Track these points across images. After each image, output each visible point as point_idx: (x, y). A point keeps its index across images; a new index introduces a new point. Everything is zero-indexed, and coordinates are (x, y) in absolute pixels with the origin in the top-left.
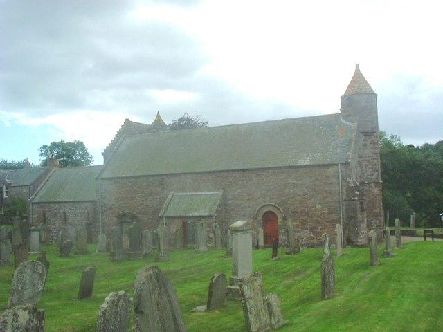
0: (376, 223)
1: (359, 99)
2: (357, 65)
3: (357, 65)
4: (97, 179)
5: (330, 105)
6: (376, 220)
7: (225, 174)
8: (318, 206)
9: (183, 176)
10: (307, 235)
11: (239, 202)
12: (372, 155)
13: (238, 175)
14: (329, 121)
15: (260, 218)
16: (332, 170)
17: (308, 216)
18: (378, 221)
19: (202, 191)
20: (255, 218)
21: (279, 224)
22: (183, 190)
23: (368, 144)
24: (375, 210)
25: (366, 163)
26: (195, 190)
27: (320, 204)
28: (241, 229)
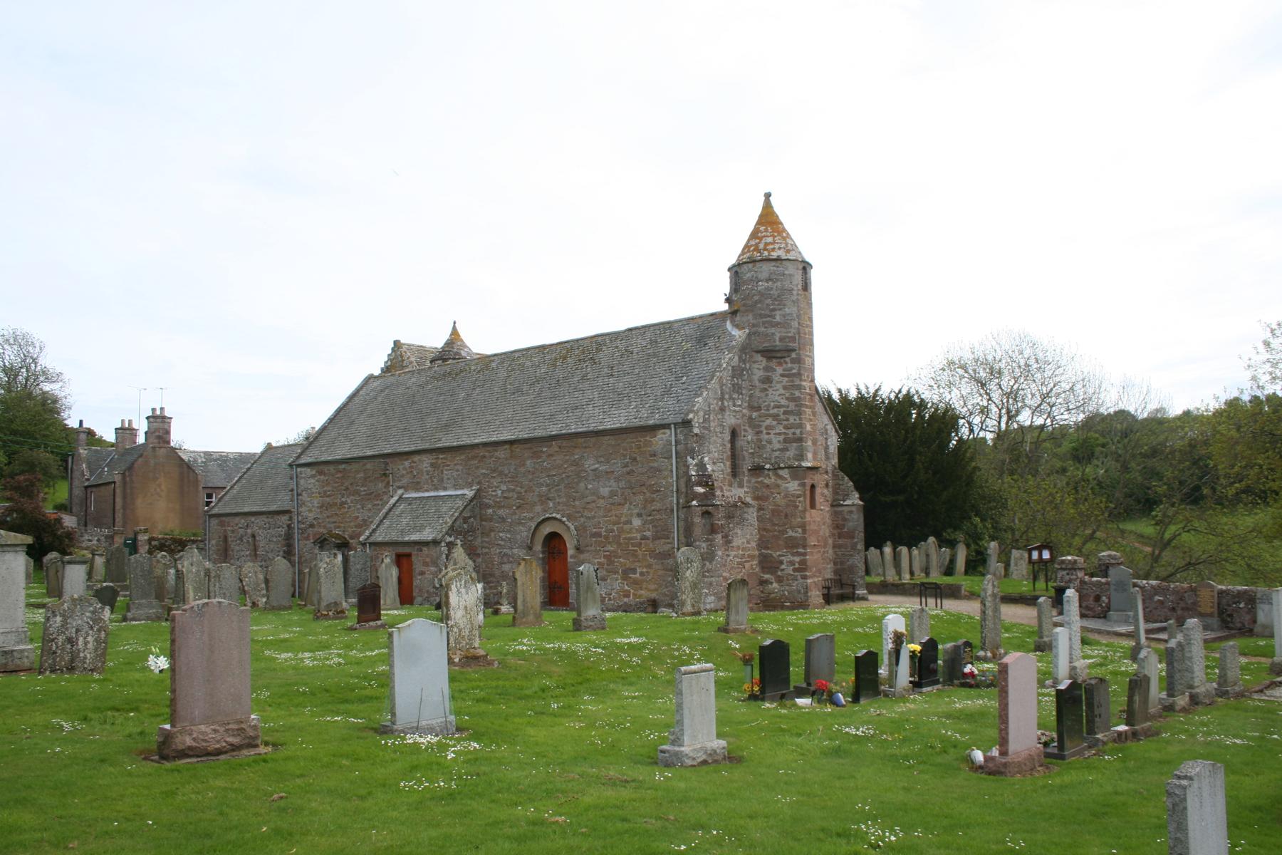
0: (792, 563)
1: (769, 284)
2: (768, 196)
3: (768, 196)
4: (290, 465)
5: (696, 287)
6: (793, 555)
7: (481, 452)
8: (637, 522)
9: (416, 458)
10: (617, 585)
11: (501, 512)
12: (783, 402)
13: (501, 453)
14: (702, 330)
15: (538, 547)
16: (662, 437)
17: (619, 544)
18: (797, 559)
19: (445, 489)
20: (530, 548)
21: (569, 560)
22: (417, 486)
23: (776, 378)
24: (790, 533)
25: (769, 421)
26: (436, 489)
27: (639, 515)
28: (924, 559)
